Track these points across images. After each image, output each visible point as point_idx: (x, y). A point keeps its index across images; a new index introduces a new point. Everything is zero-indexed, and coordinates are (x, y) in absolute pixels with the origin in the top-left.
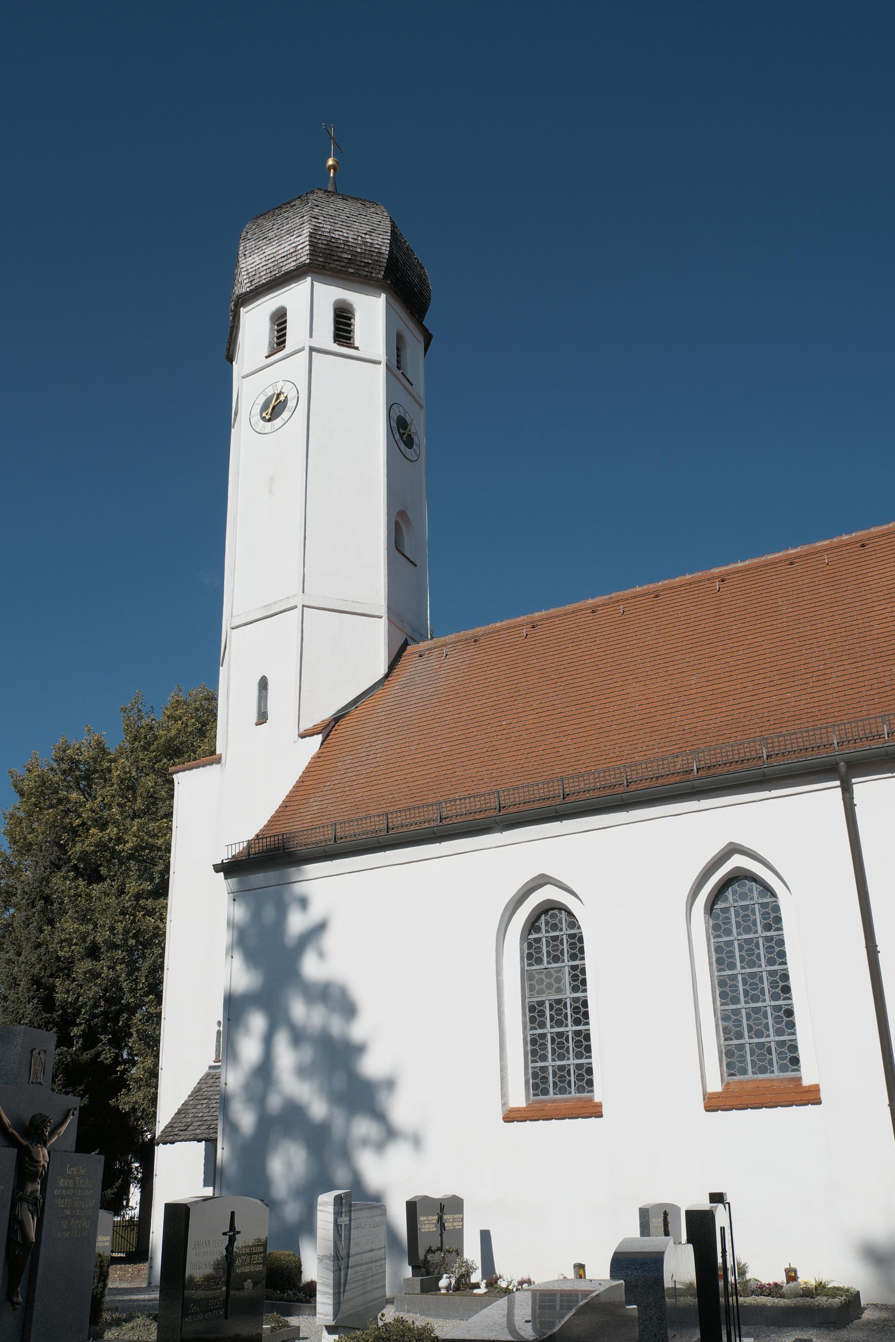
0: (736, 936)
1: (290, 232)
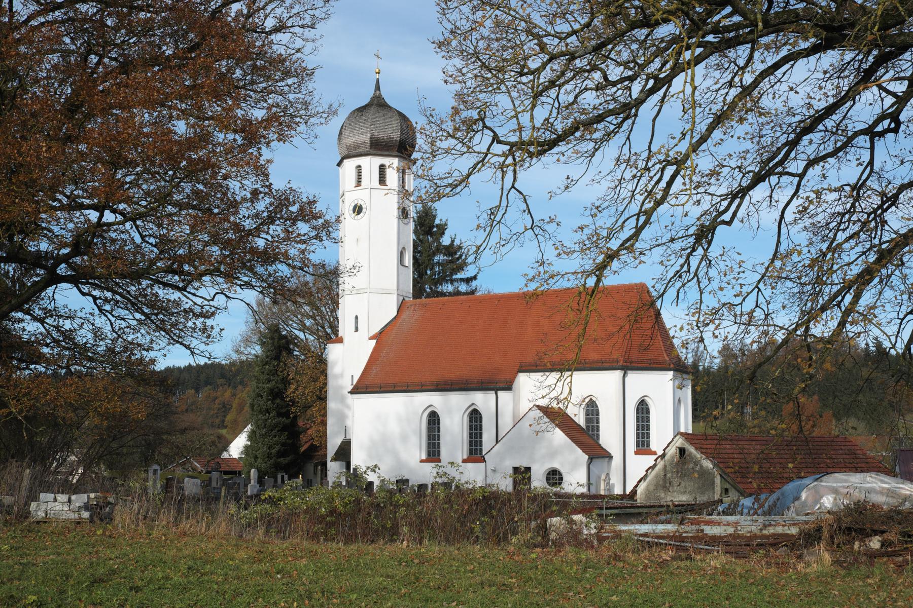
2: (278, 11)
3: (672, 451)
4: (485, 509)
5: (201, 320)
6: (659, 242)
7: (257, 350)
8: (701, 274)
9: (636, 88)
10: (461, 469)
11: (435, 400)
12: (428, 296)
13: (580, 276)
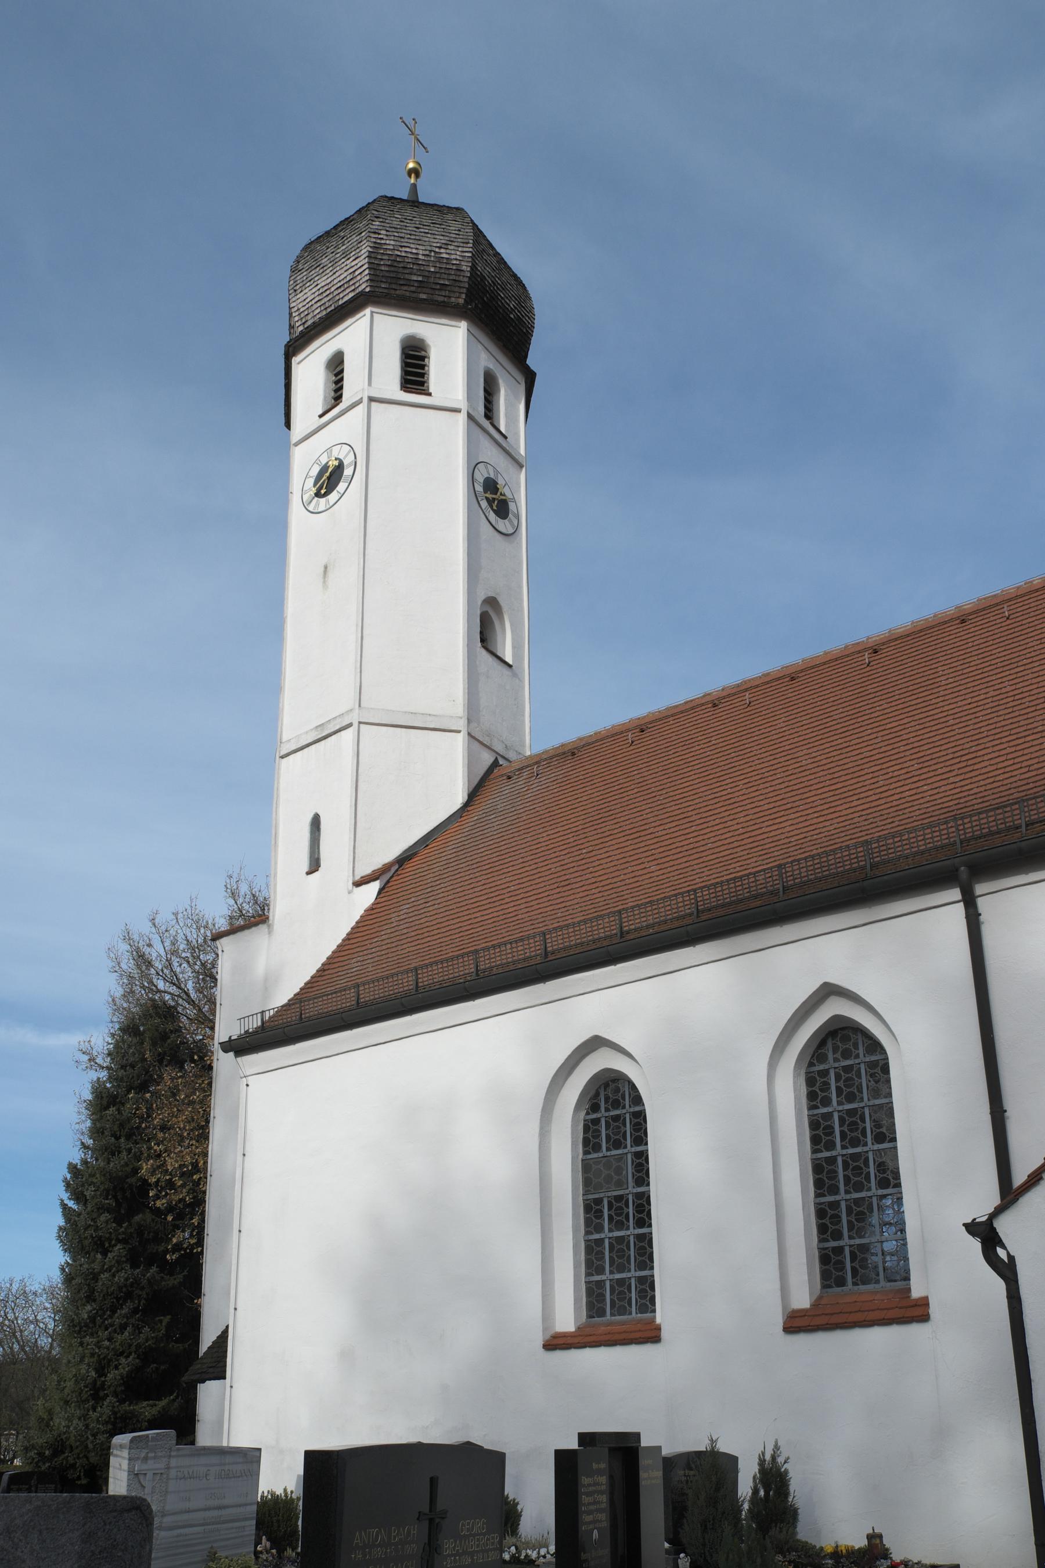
0: (835, 1107)
1: (346, 255)
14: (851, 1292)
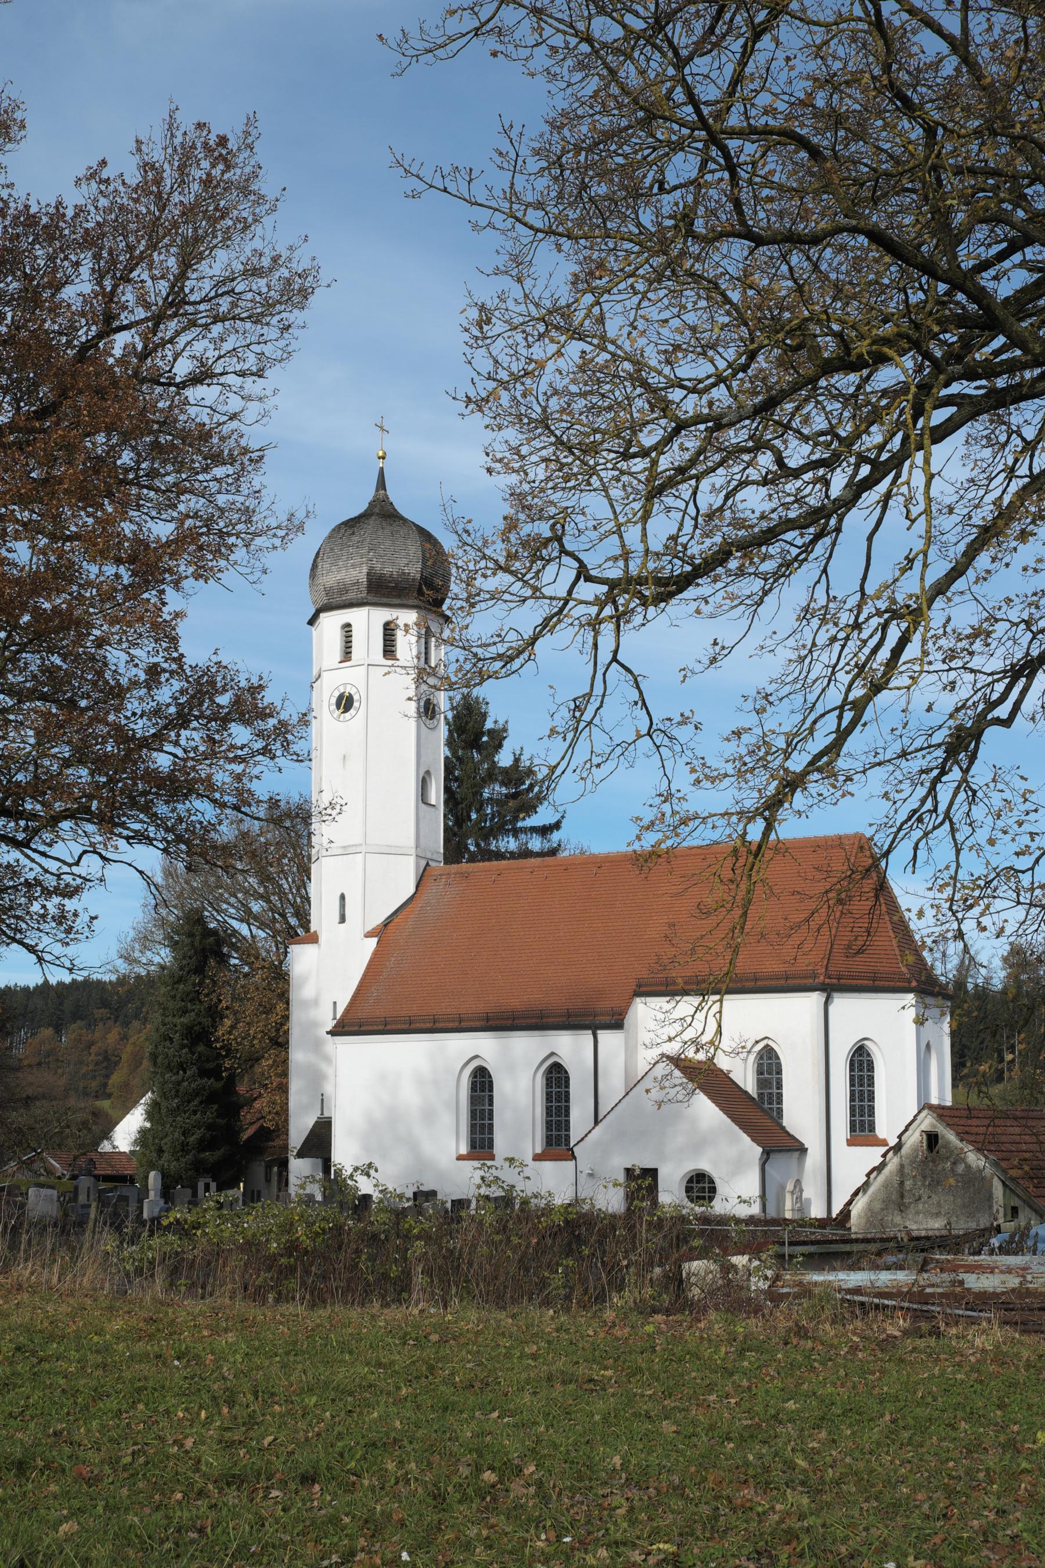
2: (199, 347)
3: (914, 1138)
4: (570, 1244)
5: (56, 900)
6: (880, 758)
7: (163, 955)
8: (957, 816)
9: (839, 482)
10: (527, 1172)
11: (484, 1046)
12: (472, 859)
13: (734, 819)
14: (556, 1150)
